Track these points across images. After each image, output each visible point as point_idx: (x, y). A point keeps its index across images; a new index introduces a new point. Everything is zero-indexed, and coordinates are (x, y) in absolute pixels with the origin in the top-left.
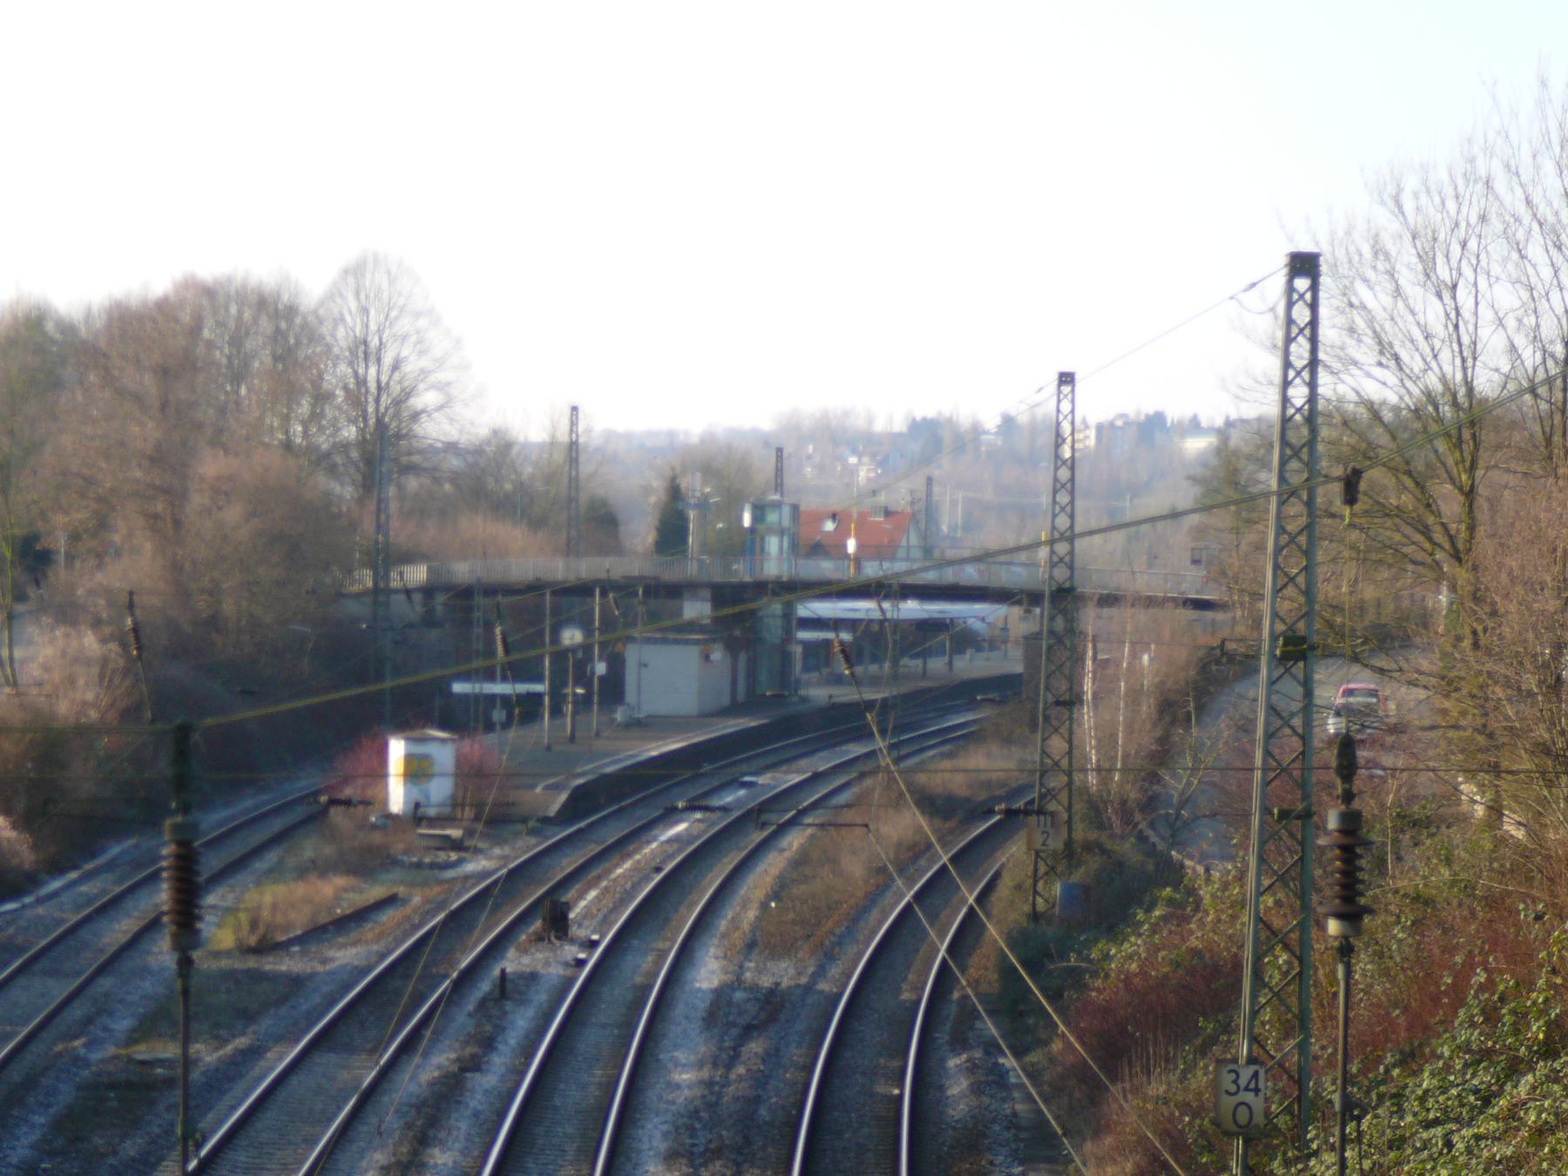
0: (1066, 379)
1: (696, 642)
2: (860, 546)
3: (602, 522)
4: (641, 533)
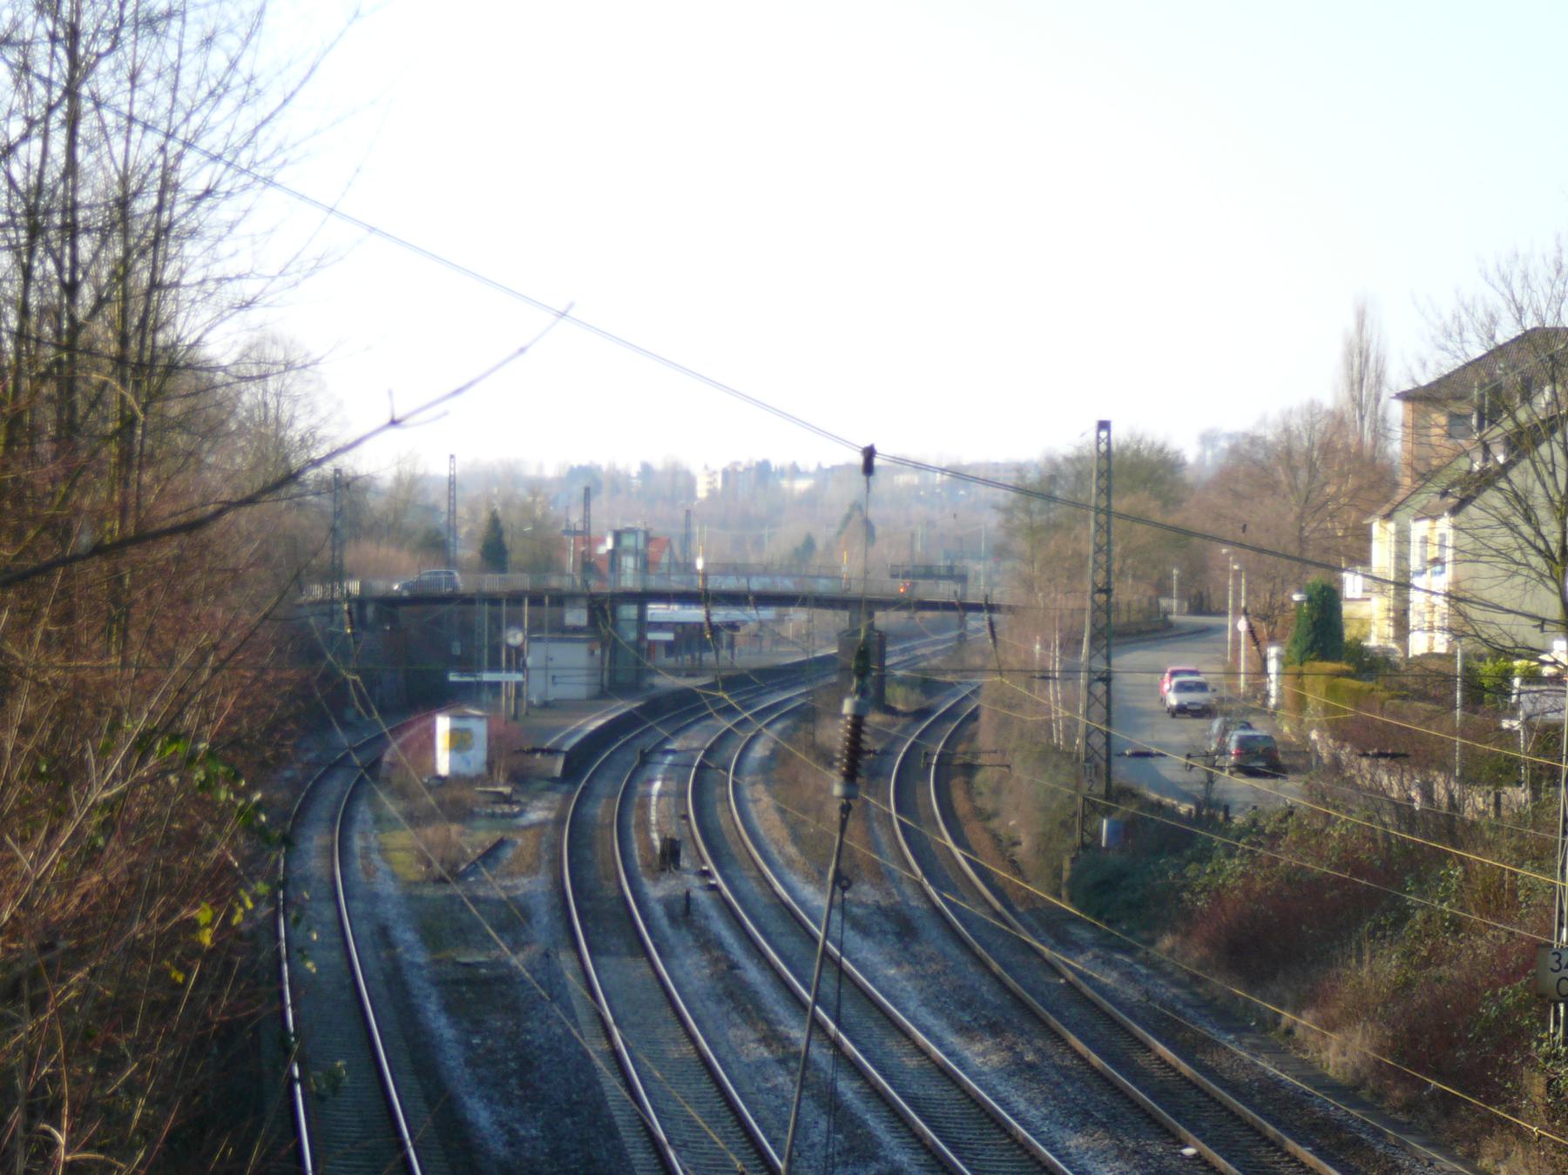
0: (1104, 425)
1: (585, 641)
2: (706, 564)
3: (436, 544)
4: (467, 551)
